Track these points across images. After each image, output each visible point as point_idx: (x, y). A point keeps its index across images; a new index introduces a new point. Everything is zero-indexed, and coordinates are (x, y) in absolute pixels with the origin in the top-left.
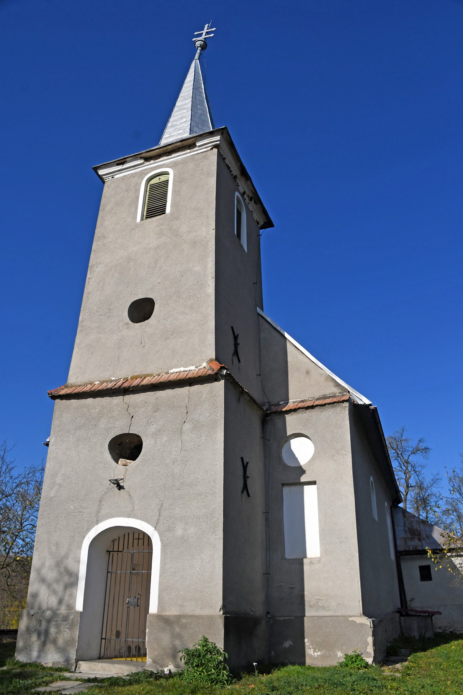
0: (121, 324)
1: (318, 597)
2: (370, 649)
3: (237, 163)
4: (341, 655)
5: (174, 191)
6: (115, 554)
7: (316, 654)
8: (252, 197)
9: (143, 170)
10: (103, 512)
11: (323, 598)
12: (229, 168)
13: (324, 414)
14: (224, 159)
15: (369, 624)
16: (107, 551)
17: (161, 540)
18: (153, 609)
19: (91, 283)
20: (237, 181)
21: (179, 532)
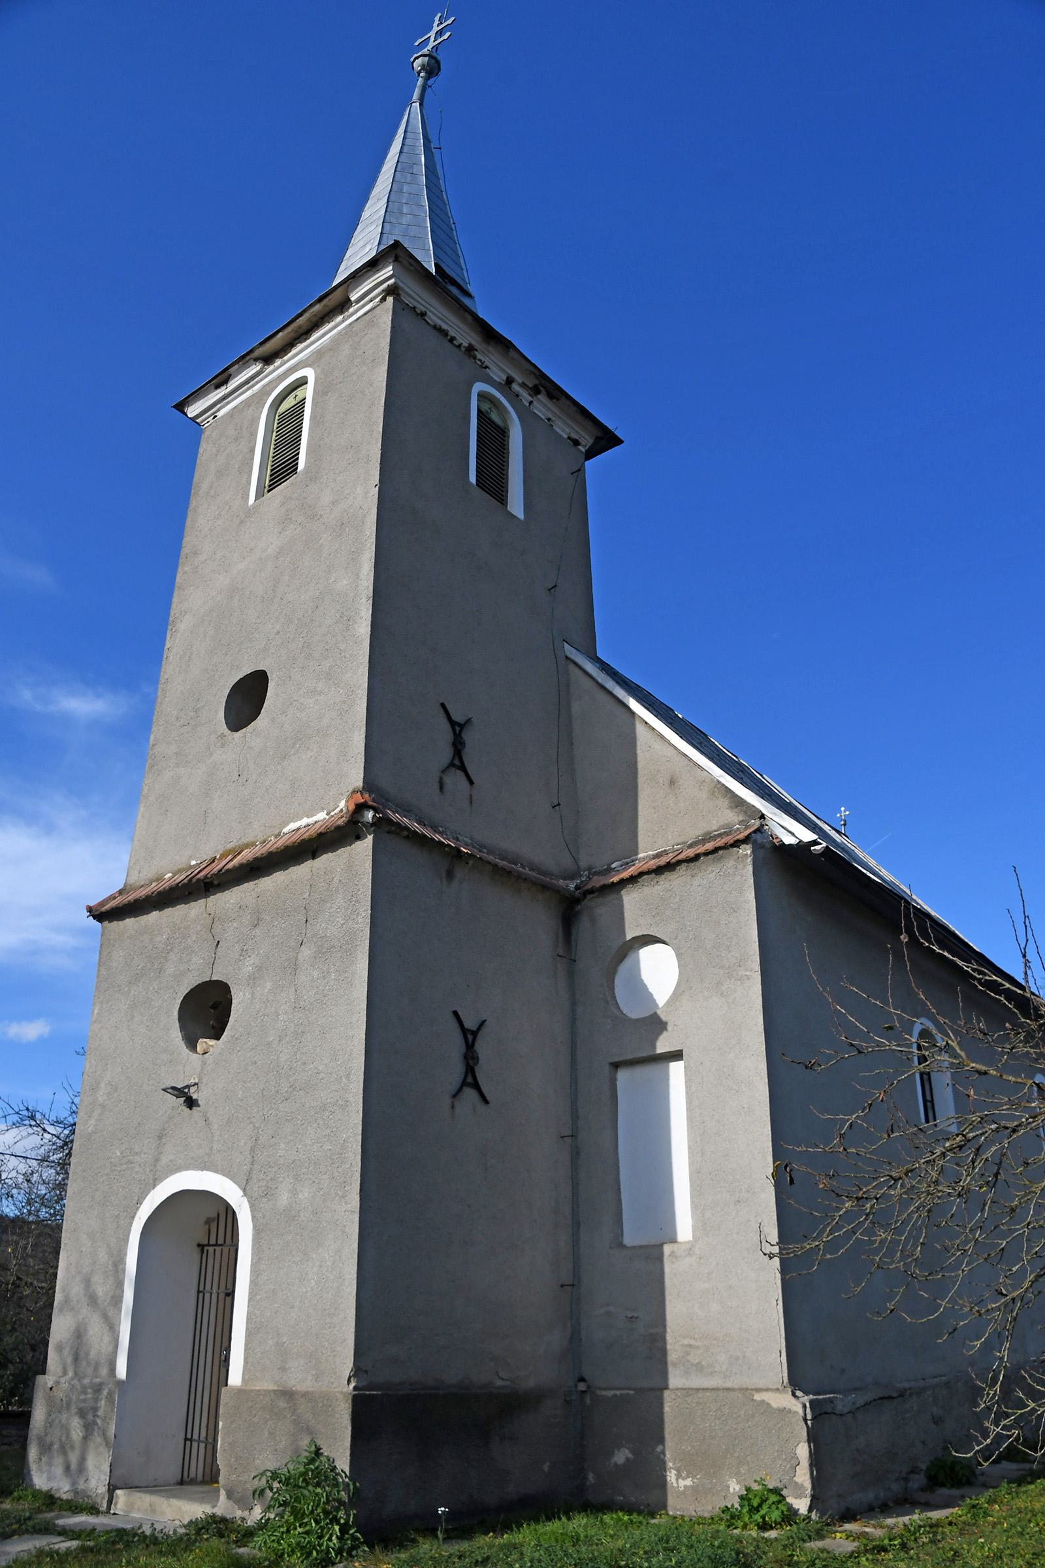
0: (213, 737)
1: (686, 1342)
2: (803, 1476)
3: (464, 320)
4: (737, 1488)
5: (312, 418)
6: (211, 1249)
7: (682, 1483)
8: (536, 386)
9: (264, 386)
10: (164, 1160)
11: (699, 1344)
12: (444, 333)
13: (697, 881)
14: (423, 314)
15: (800, 1411)
16: (199, 1245)
17: (253, 1217)
18: (235, 1377)
19: (171, 658)
20: (479, 356)
21: (284, 1199)
